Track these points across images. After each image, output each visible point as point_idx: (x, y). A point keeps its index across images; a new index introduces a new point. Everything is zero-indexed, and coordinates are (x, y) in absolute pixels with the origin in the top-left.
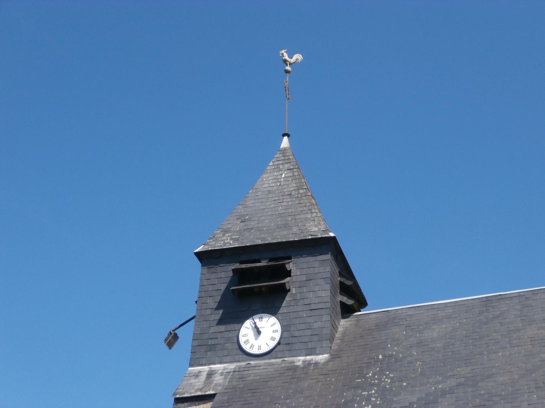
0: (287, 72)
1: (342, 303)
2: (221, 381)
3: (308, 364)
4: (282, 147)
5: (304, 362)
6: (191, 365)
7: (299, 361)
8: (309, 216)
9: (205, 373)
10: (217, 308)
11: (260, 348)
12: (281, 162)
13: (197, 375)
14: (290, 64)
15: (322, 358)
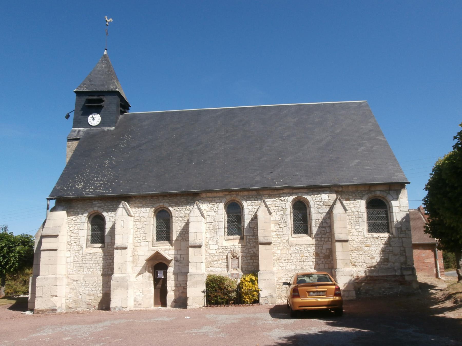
0: (107, 25)
1: (121, 111)
2: (82, 134)
3: (108, 130)
4: (104, 54)
5: (107, 129)
6: (73, 128)
7: (106, 129)
8: (111, 82)
9: (77, 131)
10: (81, 110)
11: (94, 124)
12: (103, 60)
13: (75, 131)
14: (108, 22)
15: (113, 128)
